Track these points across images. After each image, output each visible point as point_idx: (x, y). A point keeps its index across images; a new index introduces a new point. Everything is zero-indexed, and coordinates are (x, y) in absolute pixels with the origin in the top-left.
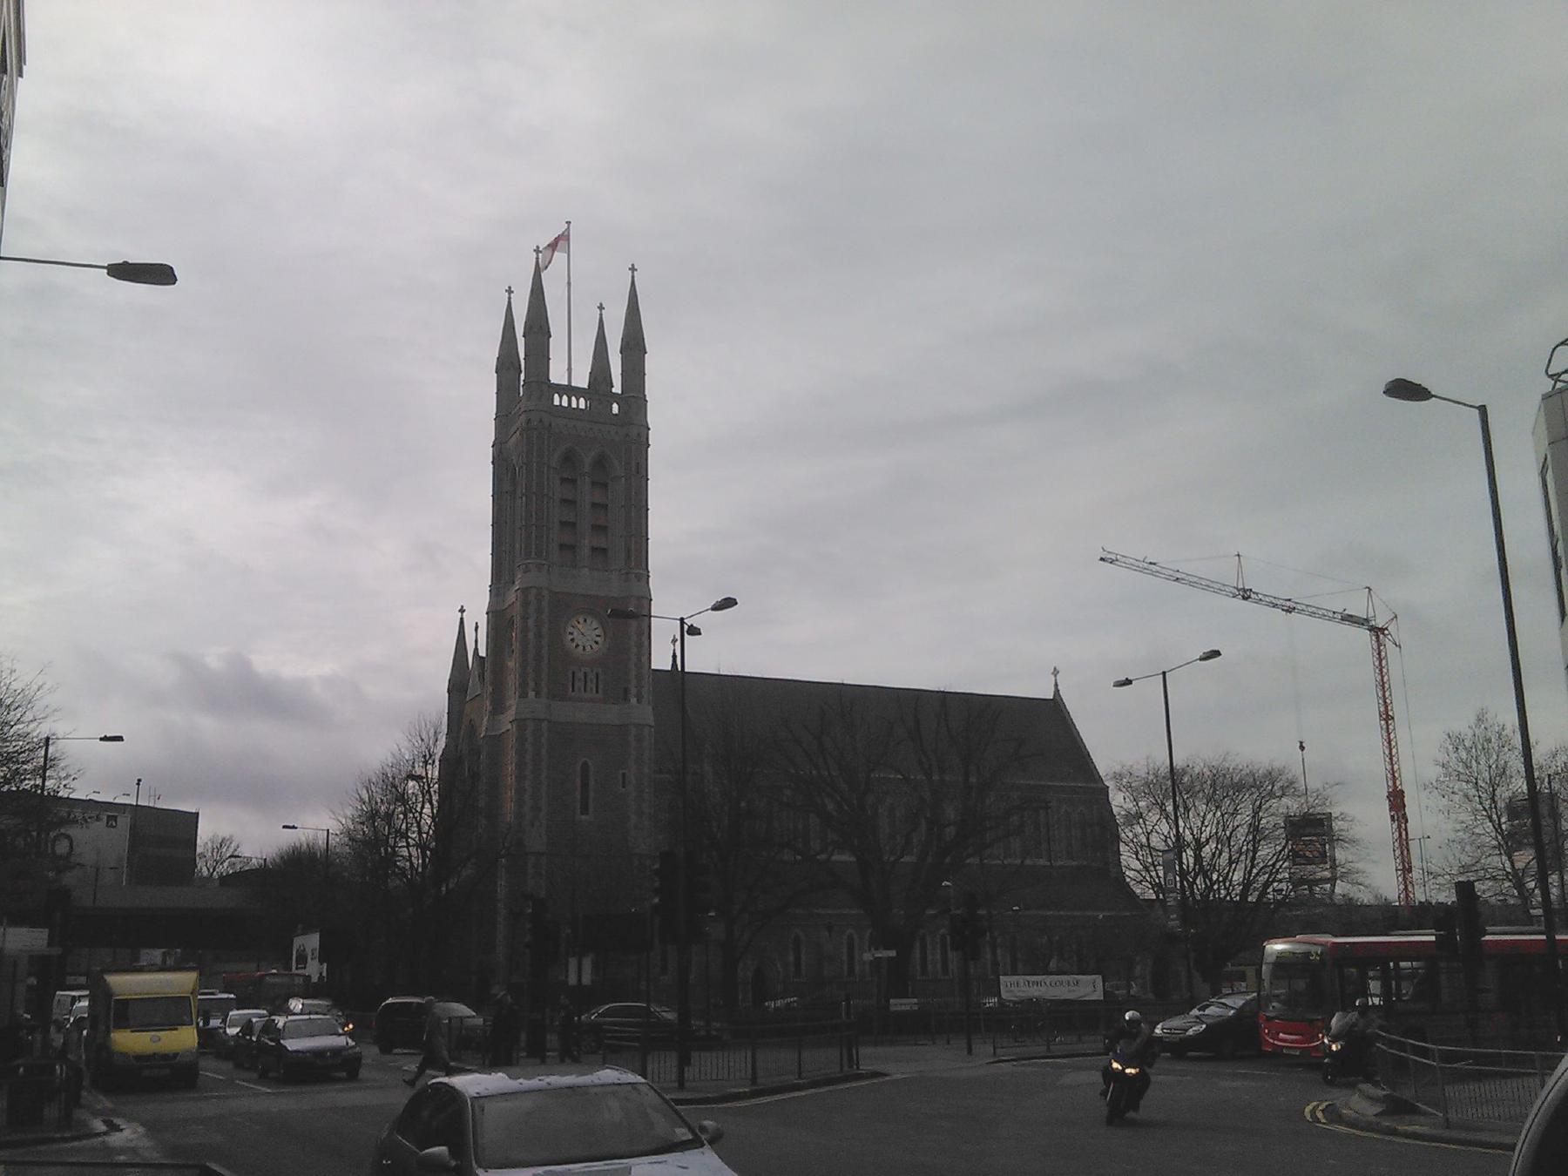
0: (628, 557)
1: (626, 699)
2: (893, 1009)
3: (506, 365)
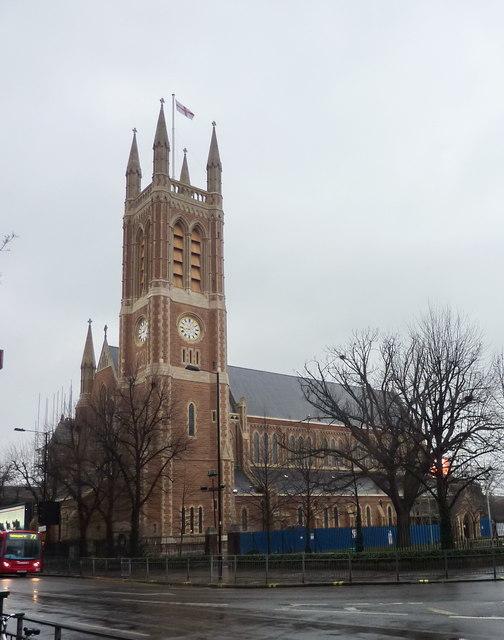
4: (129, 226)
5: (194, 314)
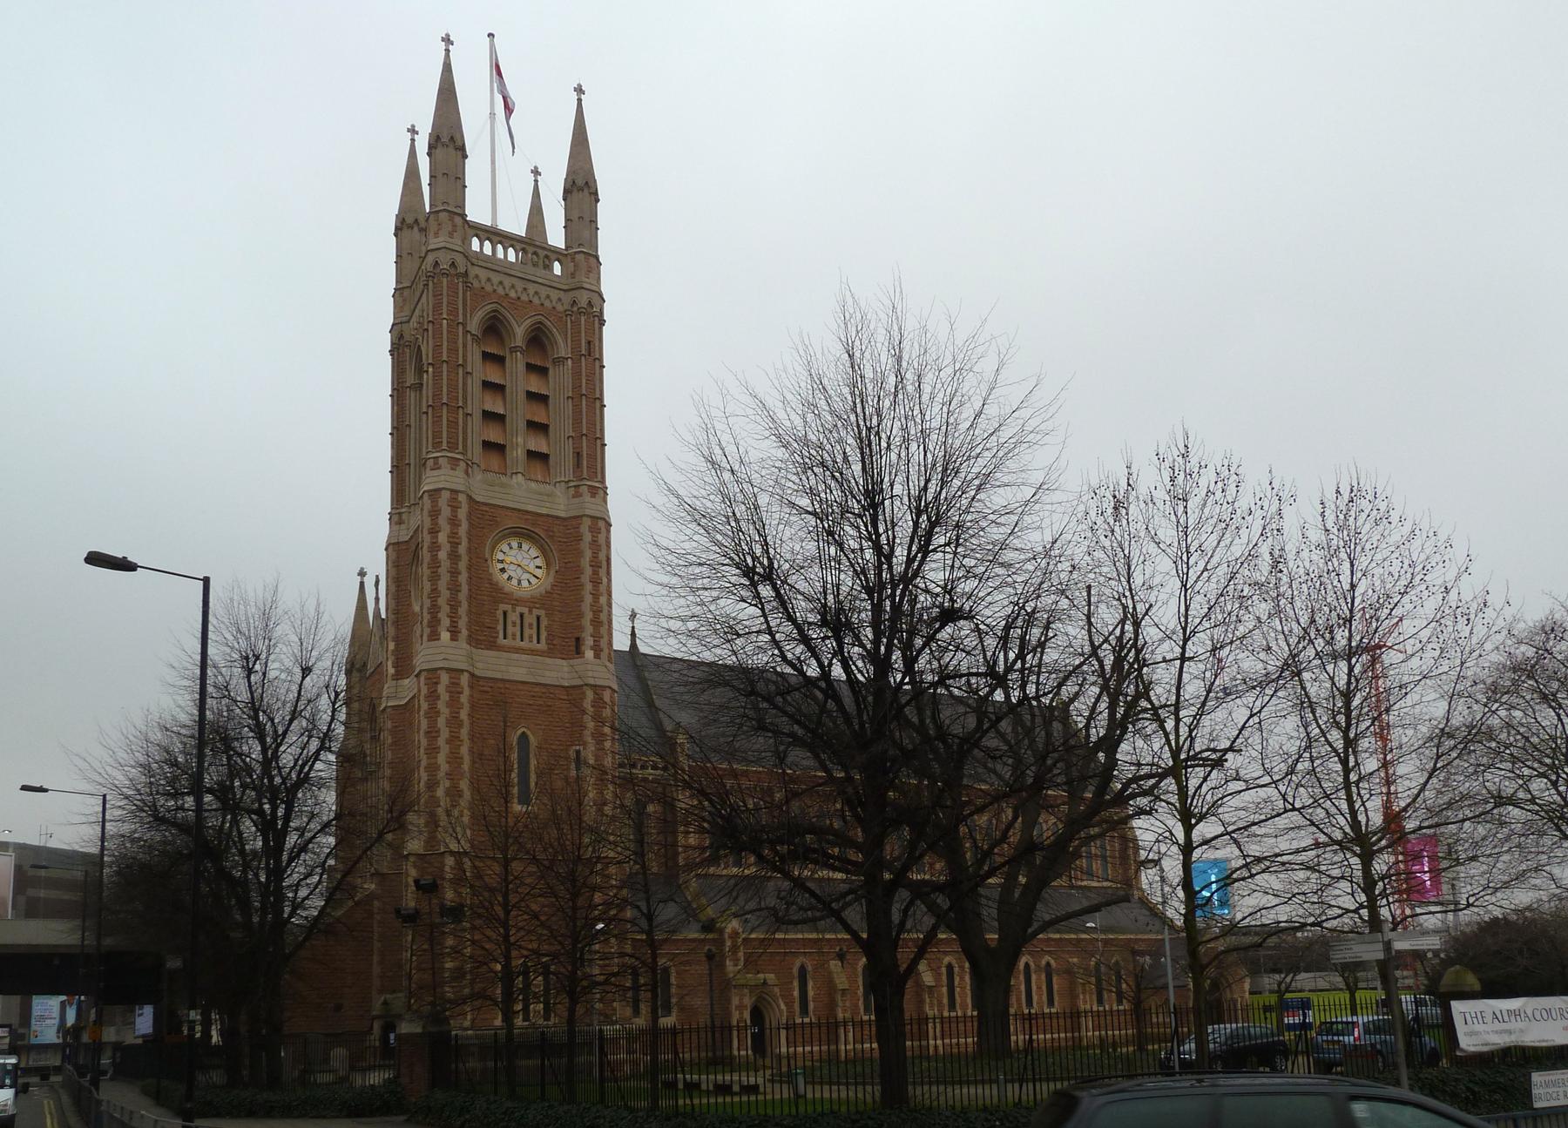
0: (578, 465)
1: (578, 652)
2: (1468, 1042)
3: (408, 224)
4: (403, 347)
5: (531, 529)
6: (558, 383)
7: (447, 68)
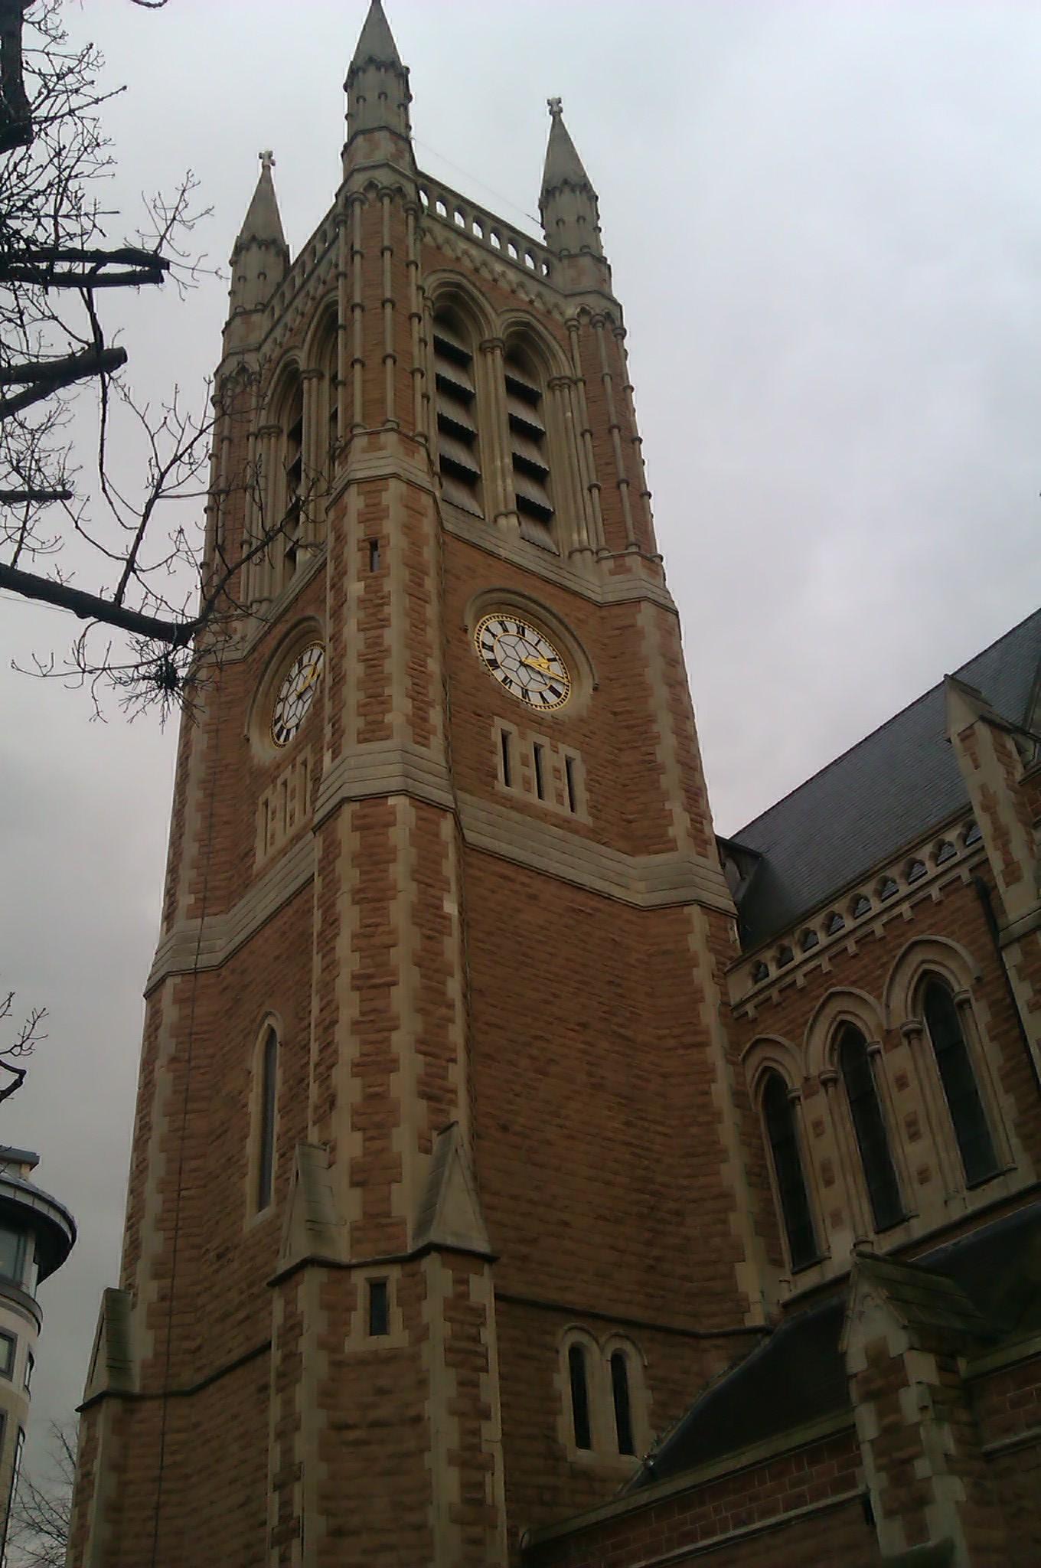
6: (560, 413)
7: (266, 181)
